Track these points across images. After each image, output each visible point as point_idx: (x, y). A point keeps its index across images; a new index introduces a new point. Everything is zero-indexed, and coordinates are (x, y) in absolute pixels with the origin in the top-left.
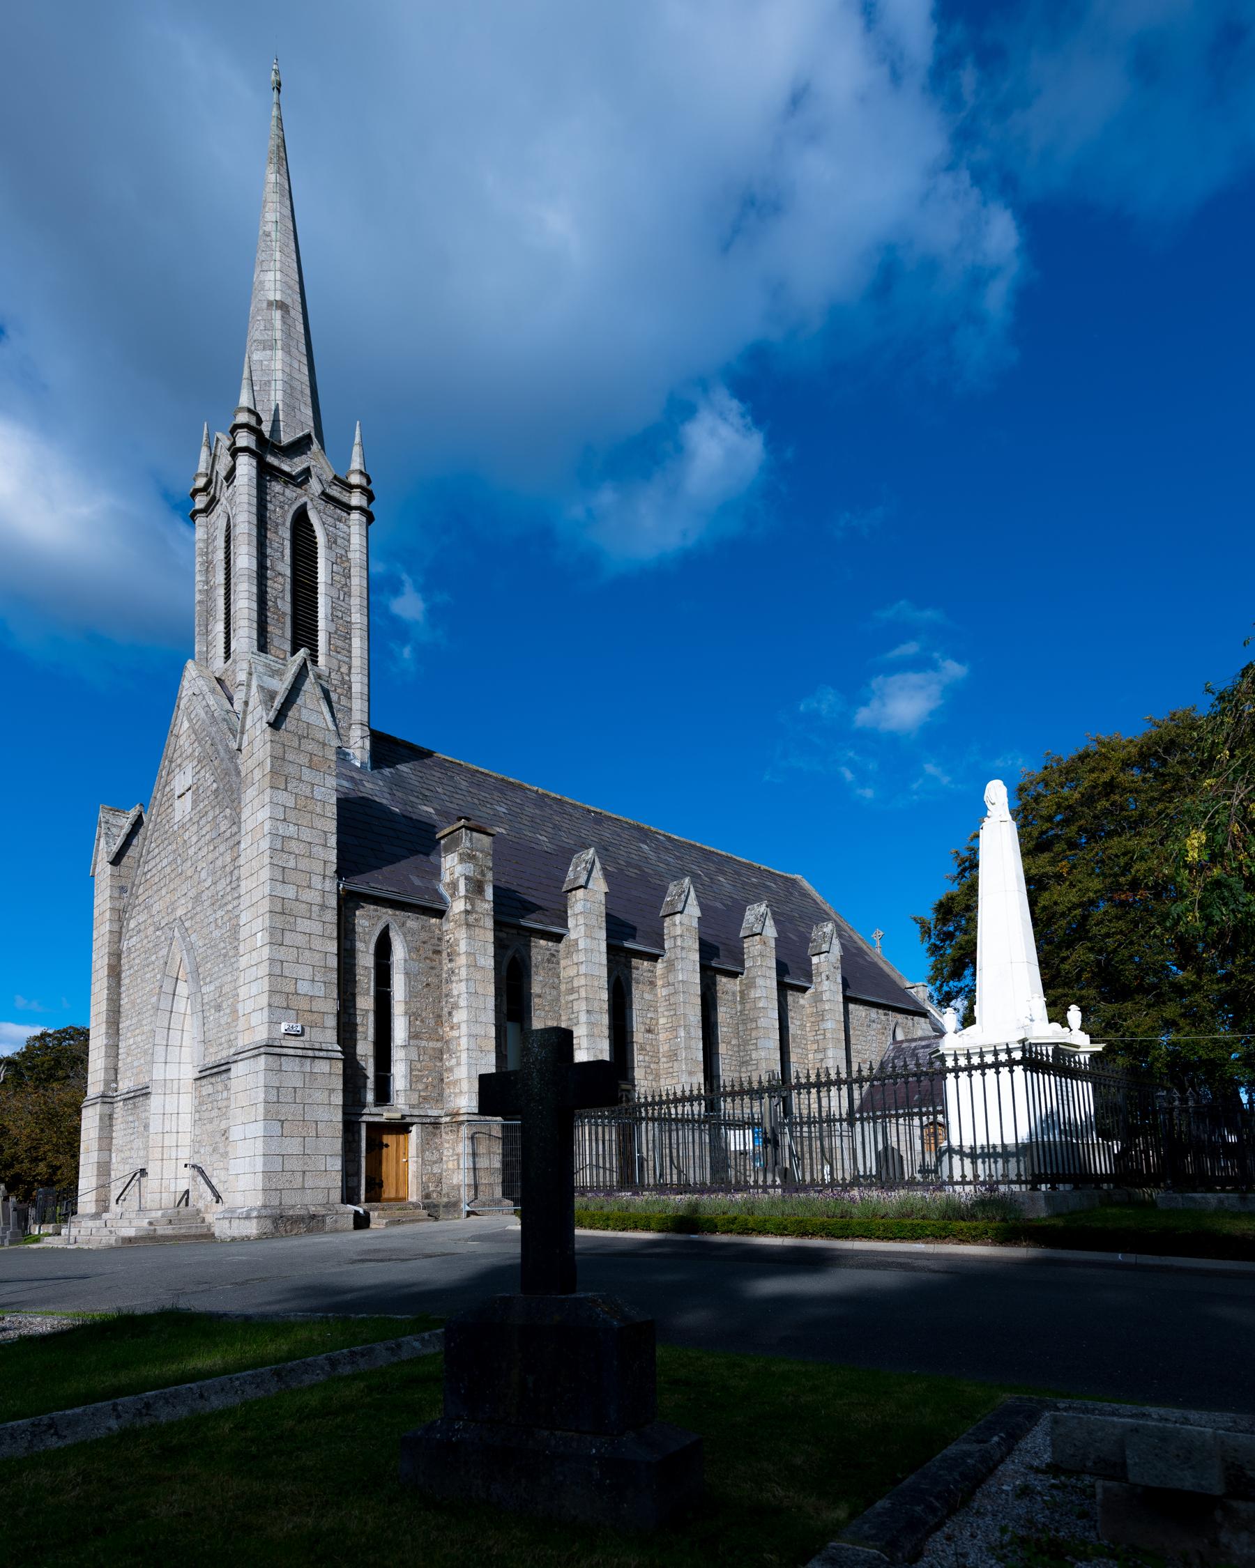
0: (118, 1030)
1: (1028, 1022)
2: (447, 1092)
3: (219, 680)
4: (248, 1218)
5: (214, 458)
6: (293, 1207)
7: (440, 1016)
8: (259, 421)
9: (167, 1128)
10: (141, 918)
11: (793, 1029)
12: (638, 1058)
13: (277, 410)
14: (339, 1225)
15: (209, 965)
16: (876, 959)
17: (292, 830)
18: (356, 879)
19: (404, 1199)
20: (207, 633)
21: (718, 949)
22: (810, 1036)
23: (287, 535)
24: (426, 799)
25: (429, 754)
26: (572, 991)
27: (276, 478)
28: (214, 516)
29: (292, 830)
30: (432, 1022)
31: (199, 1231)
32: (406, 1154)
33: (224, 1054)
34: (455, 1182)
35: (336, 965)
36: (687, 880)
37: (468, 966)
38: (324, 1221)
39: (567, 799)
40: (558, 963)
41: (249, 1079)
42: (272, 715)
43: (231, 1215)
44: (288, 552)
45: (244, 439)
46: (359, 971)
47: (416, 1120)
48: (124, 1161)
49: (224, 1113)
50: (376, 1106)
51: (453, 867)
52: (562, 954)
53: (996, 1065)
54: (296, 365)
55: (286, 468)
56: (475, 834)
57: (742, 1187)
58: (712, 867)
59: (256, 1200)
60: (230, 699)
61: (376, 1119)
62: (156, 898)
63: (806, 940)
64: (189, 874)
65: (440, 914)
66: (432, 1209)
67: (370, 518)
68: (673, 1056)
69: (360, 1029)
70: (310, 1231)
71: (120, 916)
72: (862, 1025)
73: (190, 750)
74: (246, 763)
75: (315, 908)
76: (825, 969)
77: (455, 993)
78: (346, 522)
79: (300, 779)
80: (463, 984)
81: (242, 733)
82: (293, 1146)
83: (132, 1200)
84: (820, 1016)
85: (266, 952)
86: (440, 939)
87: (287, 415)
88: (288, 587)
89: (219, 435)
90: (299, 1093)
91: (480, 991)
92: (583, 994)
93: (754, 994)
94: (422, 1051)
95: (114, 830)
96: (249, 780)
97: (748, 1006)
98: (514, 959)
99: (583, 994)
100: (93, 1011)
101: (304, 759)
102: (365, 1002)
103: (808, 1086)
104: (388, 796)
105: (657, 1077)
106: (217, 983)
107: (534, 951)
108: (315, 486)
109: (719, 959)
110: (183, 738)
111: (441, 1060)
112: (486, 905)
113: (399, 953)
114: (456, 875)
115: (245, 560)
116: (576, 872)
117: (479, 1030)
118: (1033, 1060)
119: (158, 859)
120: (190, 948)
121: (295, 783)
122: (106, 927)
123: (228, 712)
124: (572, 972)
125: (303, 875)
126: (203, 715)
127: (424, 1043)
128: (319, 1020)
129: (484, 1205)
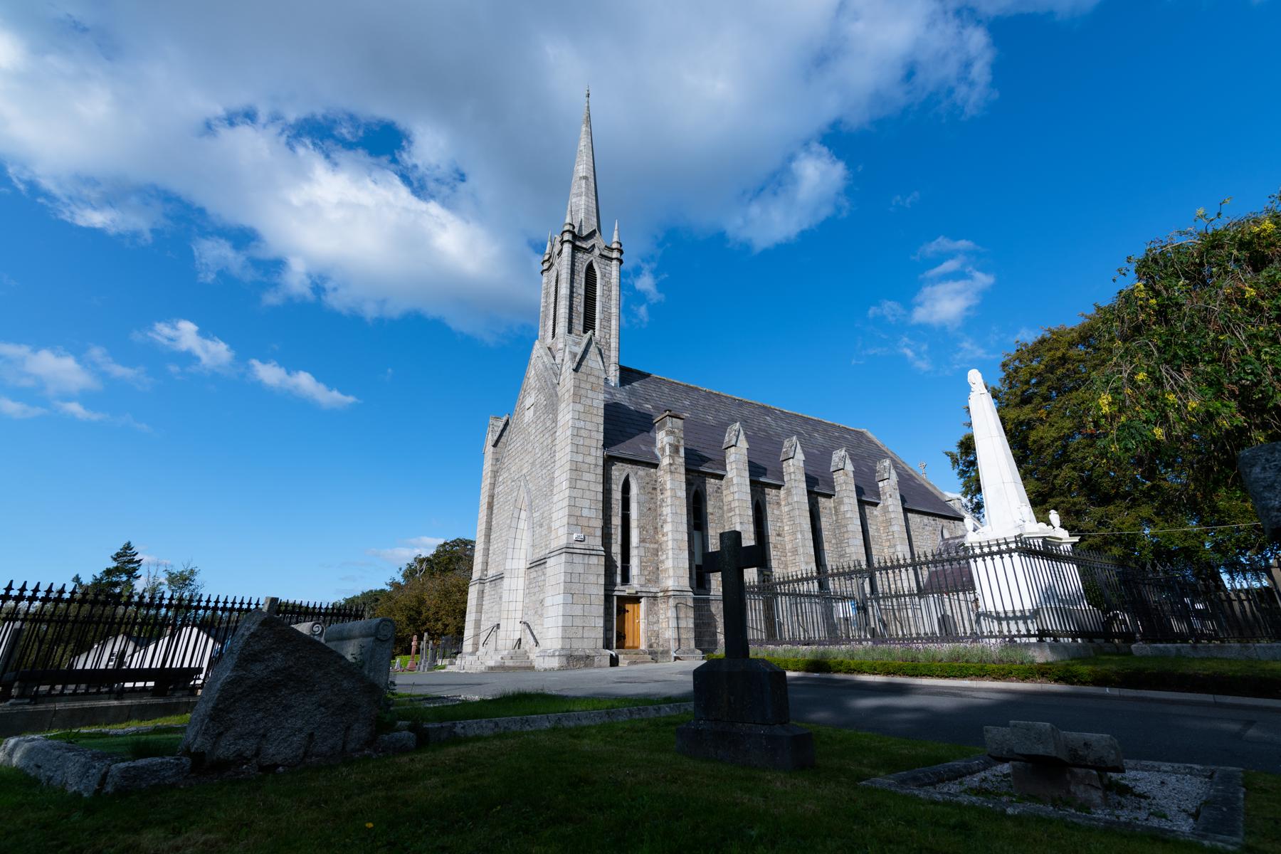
5: (553, 246)
11: (872, 532)
12: (773, 553)
18: (612, 448)
25: (648, 375)
26: (731, 510)
41: (556, 567)
43: (544, 655)
45: (567, 237)
48: (488, 619)
49: (542, 589)
51: (663, 439)
58: (810, 428)
65: (656, 466)
66: (654, 655)
67: (621, 262)
68: (795, 551)
70: (586, 666)
71: (495, 474)
74: (561, 390)
82: (578, 610)
84: (889, 522)
85: (567, 493)
98: (696, 492)
101: (588, 386)
102: (617, 521)
103: (886, 568)
105: (786, 566)
108: (597, 252)
109: (818, 488)
112: (681, 460)
115: (564, 290)
116: (729, 437)
117: (679, 536)
120: (529, 492)
122: (488, 481)
124: (730, 498)
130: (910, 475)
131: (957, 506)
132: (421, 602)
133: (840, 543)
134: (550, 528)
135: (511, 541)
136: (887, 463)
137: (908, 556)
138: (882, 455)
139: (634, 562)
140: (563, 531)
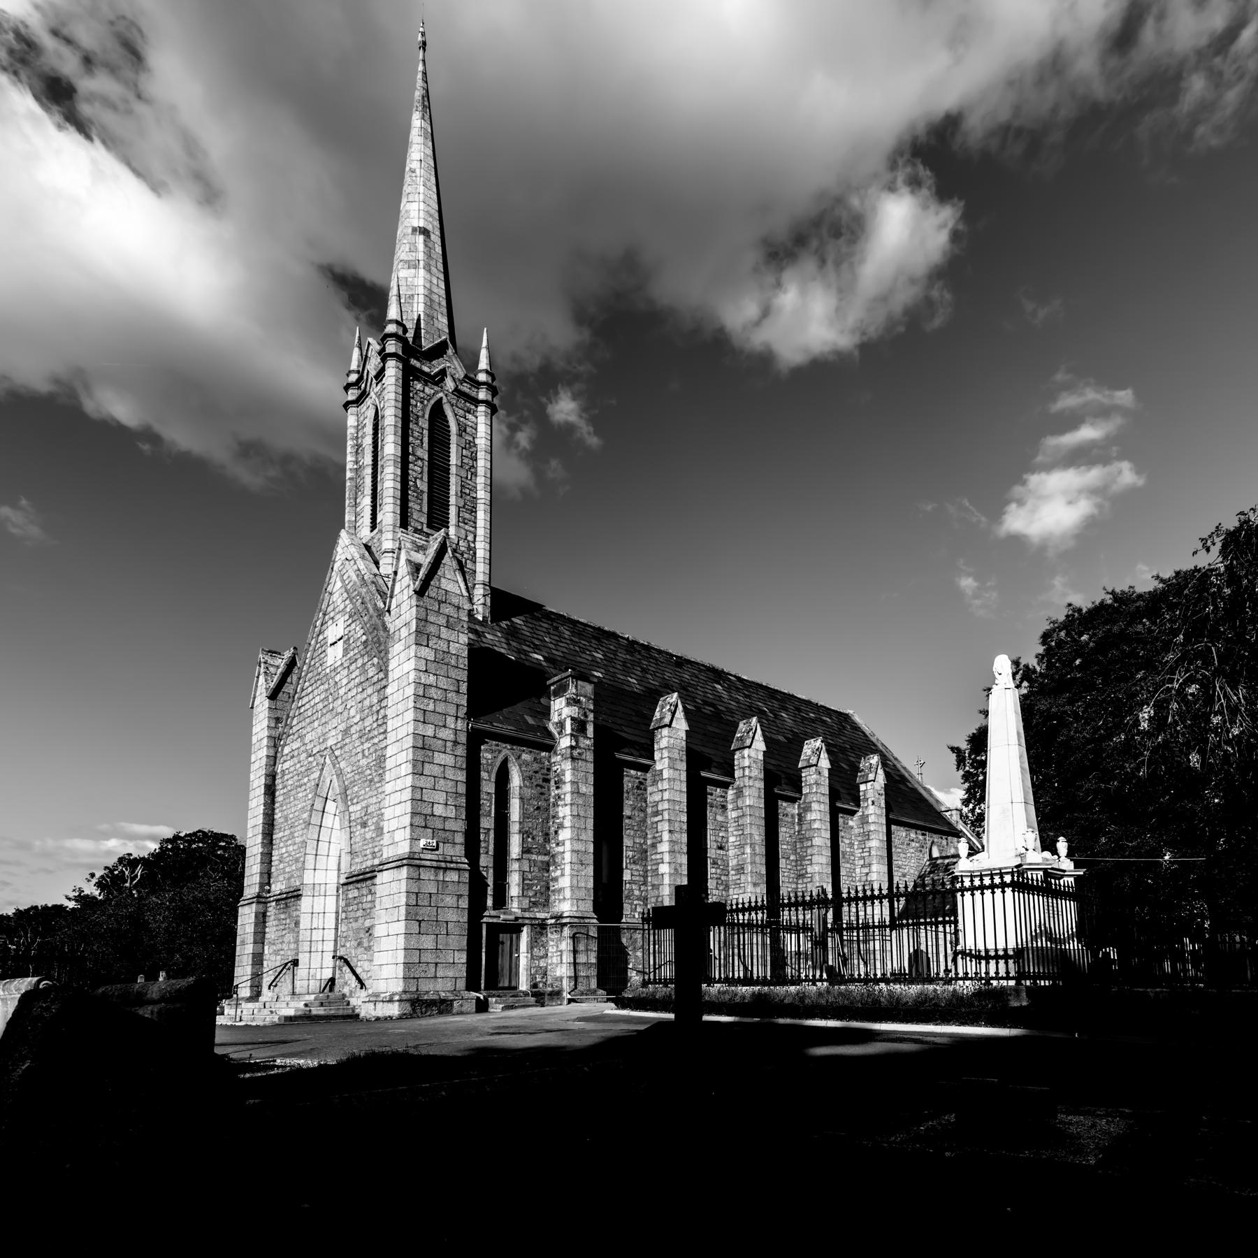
0: (272, 840)
1: (1023, 851)
2: (552, 898)
3: (368, 547)
4: (391, 1001)
5: (365, 359)
6: (427, 992)
7: (547, 834)
8: (405, 330)
9: (315, 926)
11: (843, 847)
14: (464, 1009)
15: (356, 789)
16: (916, 786)
17: (432, 679)
19: (516, 988)
20: (356, 505)
22: (858, 853)
23: (426, 426)
24: (537, 648)
26: (657, 813)
28: (363, 408)
29: (432, 679)
31: (346, 1012)
32: (518, 950)
33: (369, 863)
34: (558, 974)
36: (754, 719)
37: (572, 793)
38: (452, 1005)
41: (392, 889)
43: (375, 999)
44: (426, 440)
45: (392, 347)
46: (483, 796)
48: (276, 953)
49: (368, 913)
50: (494, 909)
51: (561, 710)
52: (649, 782)
53: (992, 887)
54: (435, 281)
55: (426, 369)
57: (797, 981)
58: (776, 704)
59: (398, 987)
60: (377, 563)
61: (495, 920)
62: (309, 729)
63: (856, 769)
64: (340, 710)
66: (540, 996)
67: (493, 410)
68: (740, 869)
69: (483, 845)
70: (441, 1013)
71: (276, 742)
73: (342, 606)
74: (392, 622)
75: (449, 744)
76: (870, 794)
77: (561, 815)
78: (474, 413)
79: (439, 637)
80: (568, 808)
81: (391, 597)
82: (428, 942)
83: (285, 986)
84: (867, 836)
85: (409, 781)
86: (549, 770)
87: (427, 323)
88: (426, 469)
89: (370, 340)
90: (434, 898)
91: (582, 813)
92: (666, 817)
93: (809, 816)
95: (272, 669)
96: (397, 637)
97: (804, 827)
99: (666, 817)
100: (250, 823)
101: (442, 621)
102: (487, 823)
103: (857, 899)
105: (727, 888)
107: (626, 779)
108: (450, 384)
109: (782, 781)
110: (335, 597)
111: (548, 871)
113: (516, 780)
114: (564, 716)
115: (390, 447)
116: (661, 712)
117: (580, 847)
118: (1020, 882)
119: (311, 696)
120: (340, 774)
121: (435, 640)
122: (264, 752)
123: (375, 575)
124: (657, 797)
125: (439, 717)
126: (354, 578)
127: (534, 857)
128: (450, 837)
129: (582, 994)
130: (902, 777)
131: (954, 818)
133: (801, 860)
134: (379, 830)
136: (875, 760)
137: (885, 886)
138: (869, 746)
139: (514, 880)
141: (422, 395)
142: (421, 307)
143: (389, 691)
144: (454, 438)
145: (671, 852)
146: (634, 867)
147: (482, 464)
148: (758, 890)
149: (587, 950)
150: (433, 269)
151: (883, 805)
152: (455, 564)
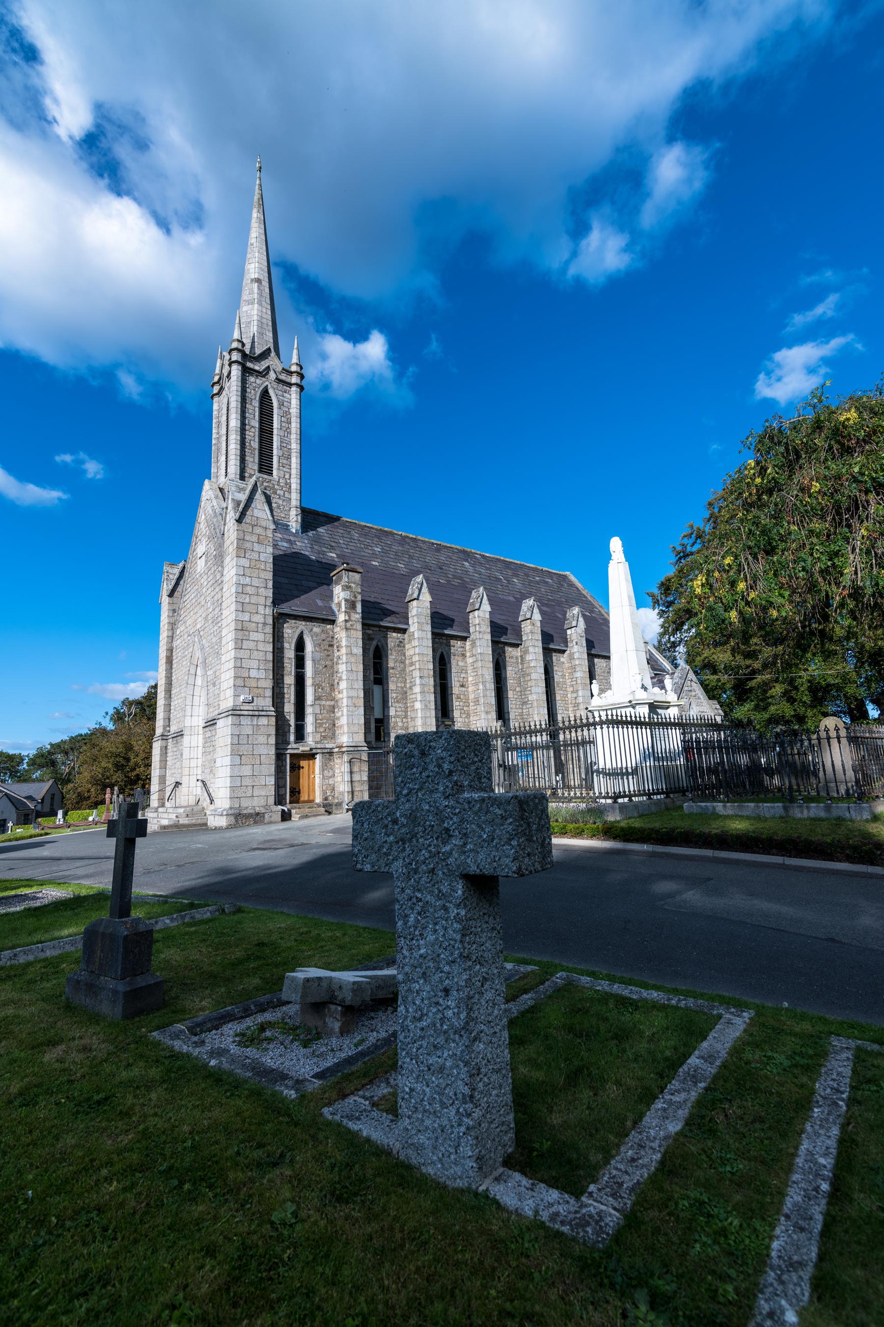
2: (337, 732)
3: (221, 490)
4: (222, 815)
6: (247, 808)
7: (333, 685)
8: (243, 345)
10: (182, 628)
11: (557, 678)
12: (456, 703)
13: (254, 336)
14: (272, 819)
18: (284, 606)
19: (313, 801)
21: (507, 629)
24: (332, 548)
25: (338, 519)
26: (412, 664)
27: (252, 374)
30: (328, 690)
35: (271, 659)
36: (481, 589)
37: (347, 654)
39: (419, 537)
40: (404, 647)
41: (225, 727)
42: (238, 515)
44: (257, 414)
45: (236, 356)
46: (286, 660)
47: (319, 751)
50: (296, 743)
51: (339, 594)
55: (257, 368)
56: (350, 573)
58: (510, 572)
61: (296, 751)
65: (333, 622)
67: (302, 388)
68: (477, 702)
69: (286, 696)
70: (256, 822)
71: (173, 626)
72: (604, 672)
75: (260, 625)
76: (574, 637)
77: (340, 670)
82: (247, 771)
84: (573, 669)
85: (232, 654)
86: (333, 638)
88: (257, 433)
94: (322, 707)
95: (171, 576)
97: (525, 666)
98: (377, 647)
102: (289, 680)
104: (309, 549)
105: (468, 716)
106: (214, 669)
107: (389, 640)
108: (272, 376)
110: (202, 524)
111: (334, 712)
112: (357, 616)
116: (412, 591)
117: (354, 693)
120: (202, 648)
125: (253, 606)
126: (211, 512)
127: (323, 703)
132: (129, 748)
135: (189, 698)
139: (309, 720)
140: (230, 693)
141: (254, 385)
142: (255, 328)
143: (224, 590)
144: (275, 411)
145: (422, 692)
146: (398, 705)
147: (295, 425)
148: (490, 717)
149: (360, 771)
150: (264, 303)
151: (584, 644)
152: (263, 498)
